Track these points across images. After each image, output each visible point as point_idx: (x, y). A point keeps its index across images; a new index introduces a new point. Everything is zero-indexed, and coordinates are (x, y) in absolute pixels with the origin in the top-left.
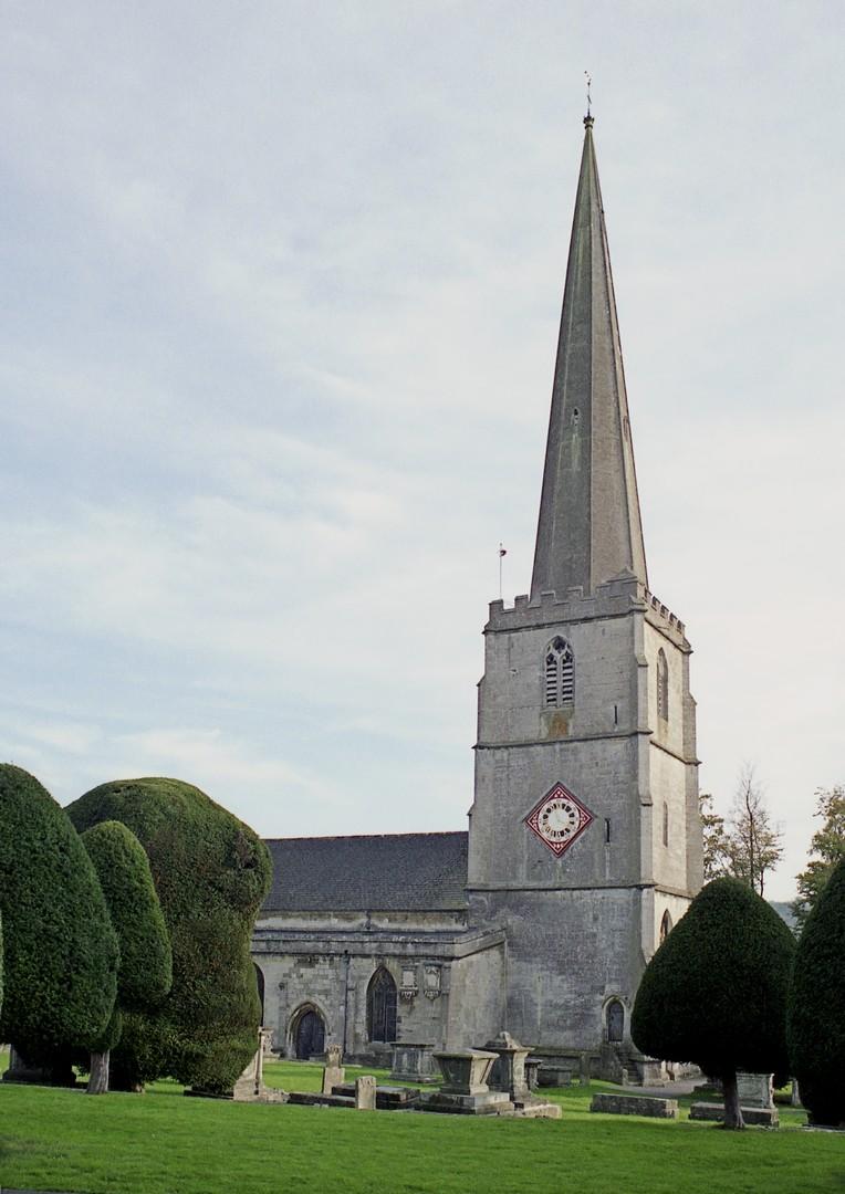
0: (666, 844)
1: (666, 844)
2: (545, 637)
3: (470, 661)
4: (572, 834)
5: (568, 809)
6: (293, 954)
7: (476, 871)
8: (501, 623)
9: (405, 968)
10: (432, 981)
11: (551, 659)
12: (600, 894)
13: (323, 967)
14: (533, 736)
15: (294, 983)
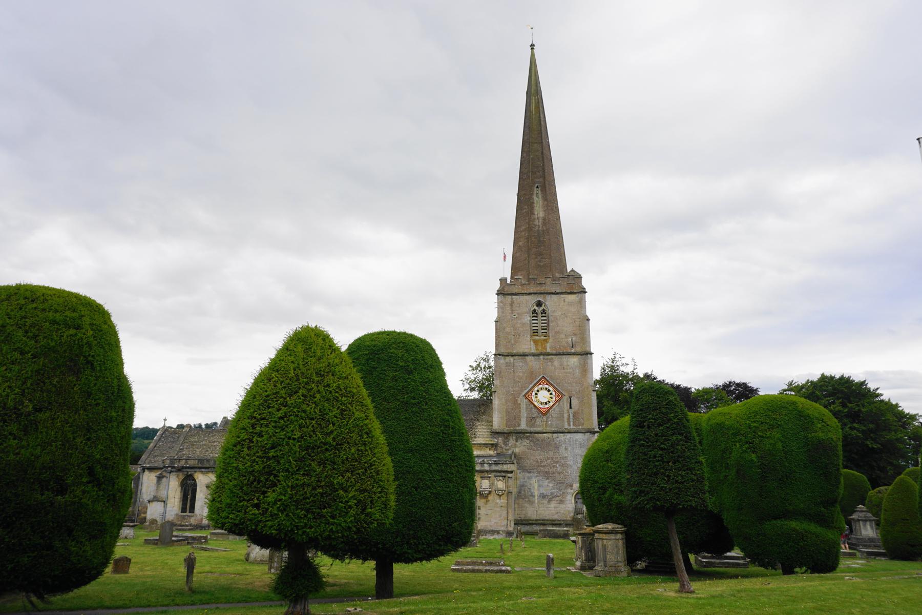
2: (533, 299)
4: (551, 404)
5: (549, 391)
9: (482, 478)
12: (569, 436)
14: (527, 351)
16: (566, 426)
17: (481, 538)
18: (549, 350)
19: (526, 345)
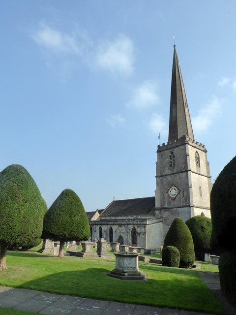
0: (201, 195)
1: (201, 195)
3: (154, 157)
6: (117, 225)
7: (158, 204)
8: (161, 150)
9: (138, 227)
10: (143, 230)
11: (170, 157)
13: (123, 227)
15: (118, 231)
16: (182, 205)
17: (43, 240)
18: (175, 172)
19: (167, 171)
